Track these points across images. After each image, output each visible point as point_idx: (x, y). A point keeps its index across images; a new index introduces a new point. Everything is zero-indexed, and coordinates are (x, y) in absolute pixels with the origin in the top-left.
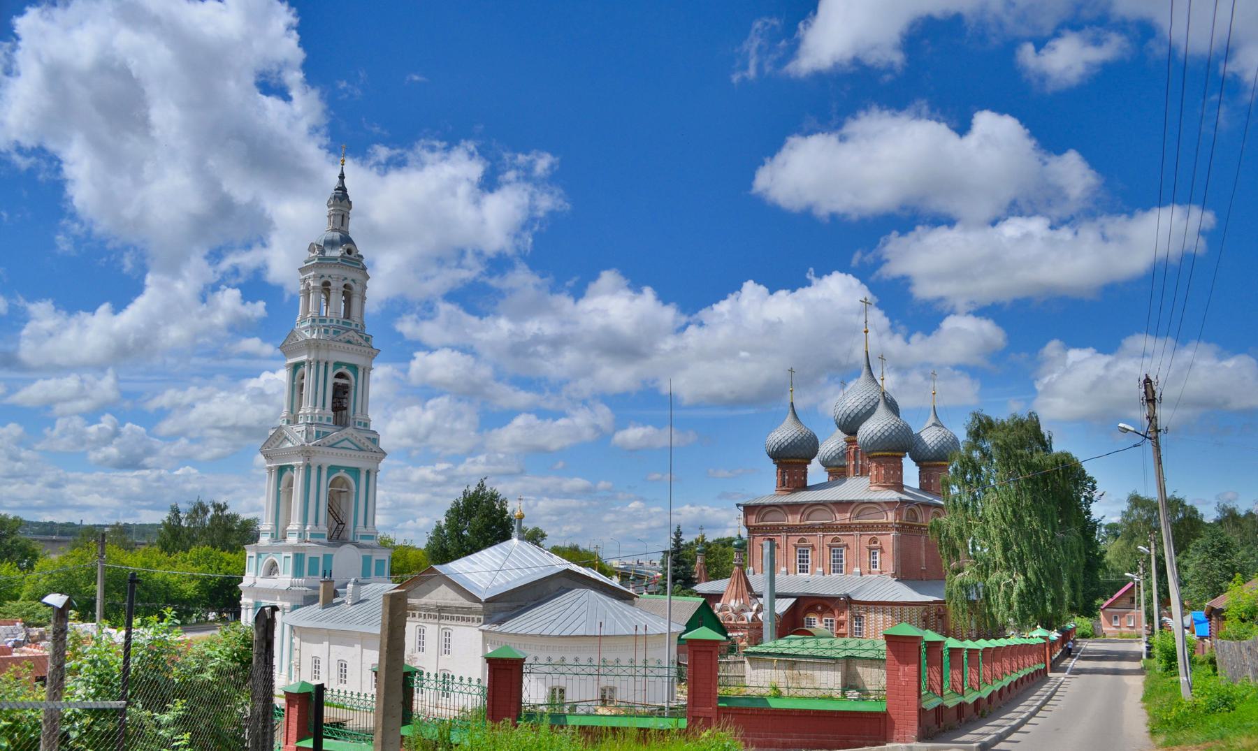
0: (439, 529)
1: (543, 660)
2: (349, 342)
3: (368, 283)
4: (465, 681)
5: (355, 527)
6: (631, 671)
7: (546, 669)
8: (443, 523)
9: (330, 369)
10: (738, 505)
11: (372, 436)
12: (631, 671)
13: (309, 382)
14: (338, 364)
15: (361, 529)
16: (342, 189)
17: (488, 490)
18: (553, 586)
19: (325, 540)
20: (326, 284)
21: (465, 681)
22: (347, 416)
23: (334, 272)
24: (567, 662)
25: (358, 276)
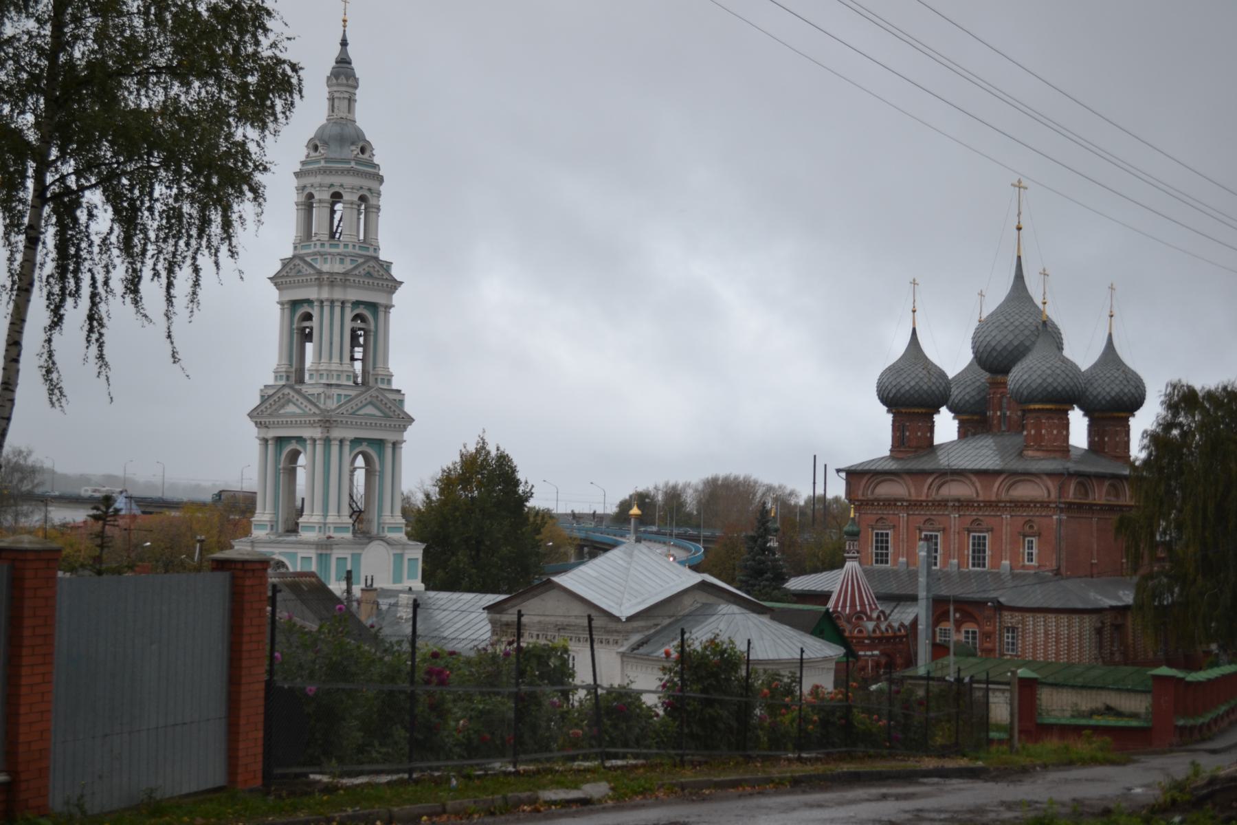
2: (369, 275)
10: (838, 471)
11: (397, 397)
14: (357, 304)
16: (343, 62)
19: (348, 535)
23: (348, 181)
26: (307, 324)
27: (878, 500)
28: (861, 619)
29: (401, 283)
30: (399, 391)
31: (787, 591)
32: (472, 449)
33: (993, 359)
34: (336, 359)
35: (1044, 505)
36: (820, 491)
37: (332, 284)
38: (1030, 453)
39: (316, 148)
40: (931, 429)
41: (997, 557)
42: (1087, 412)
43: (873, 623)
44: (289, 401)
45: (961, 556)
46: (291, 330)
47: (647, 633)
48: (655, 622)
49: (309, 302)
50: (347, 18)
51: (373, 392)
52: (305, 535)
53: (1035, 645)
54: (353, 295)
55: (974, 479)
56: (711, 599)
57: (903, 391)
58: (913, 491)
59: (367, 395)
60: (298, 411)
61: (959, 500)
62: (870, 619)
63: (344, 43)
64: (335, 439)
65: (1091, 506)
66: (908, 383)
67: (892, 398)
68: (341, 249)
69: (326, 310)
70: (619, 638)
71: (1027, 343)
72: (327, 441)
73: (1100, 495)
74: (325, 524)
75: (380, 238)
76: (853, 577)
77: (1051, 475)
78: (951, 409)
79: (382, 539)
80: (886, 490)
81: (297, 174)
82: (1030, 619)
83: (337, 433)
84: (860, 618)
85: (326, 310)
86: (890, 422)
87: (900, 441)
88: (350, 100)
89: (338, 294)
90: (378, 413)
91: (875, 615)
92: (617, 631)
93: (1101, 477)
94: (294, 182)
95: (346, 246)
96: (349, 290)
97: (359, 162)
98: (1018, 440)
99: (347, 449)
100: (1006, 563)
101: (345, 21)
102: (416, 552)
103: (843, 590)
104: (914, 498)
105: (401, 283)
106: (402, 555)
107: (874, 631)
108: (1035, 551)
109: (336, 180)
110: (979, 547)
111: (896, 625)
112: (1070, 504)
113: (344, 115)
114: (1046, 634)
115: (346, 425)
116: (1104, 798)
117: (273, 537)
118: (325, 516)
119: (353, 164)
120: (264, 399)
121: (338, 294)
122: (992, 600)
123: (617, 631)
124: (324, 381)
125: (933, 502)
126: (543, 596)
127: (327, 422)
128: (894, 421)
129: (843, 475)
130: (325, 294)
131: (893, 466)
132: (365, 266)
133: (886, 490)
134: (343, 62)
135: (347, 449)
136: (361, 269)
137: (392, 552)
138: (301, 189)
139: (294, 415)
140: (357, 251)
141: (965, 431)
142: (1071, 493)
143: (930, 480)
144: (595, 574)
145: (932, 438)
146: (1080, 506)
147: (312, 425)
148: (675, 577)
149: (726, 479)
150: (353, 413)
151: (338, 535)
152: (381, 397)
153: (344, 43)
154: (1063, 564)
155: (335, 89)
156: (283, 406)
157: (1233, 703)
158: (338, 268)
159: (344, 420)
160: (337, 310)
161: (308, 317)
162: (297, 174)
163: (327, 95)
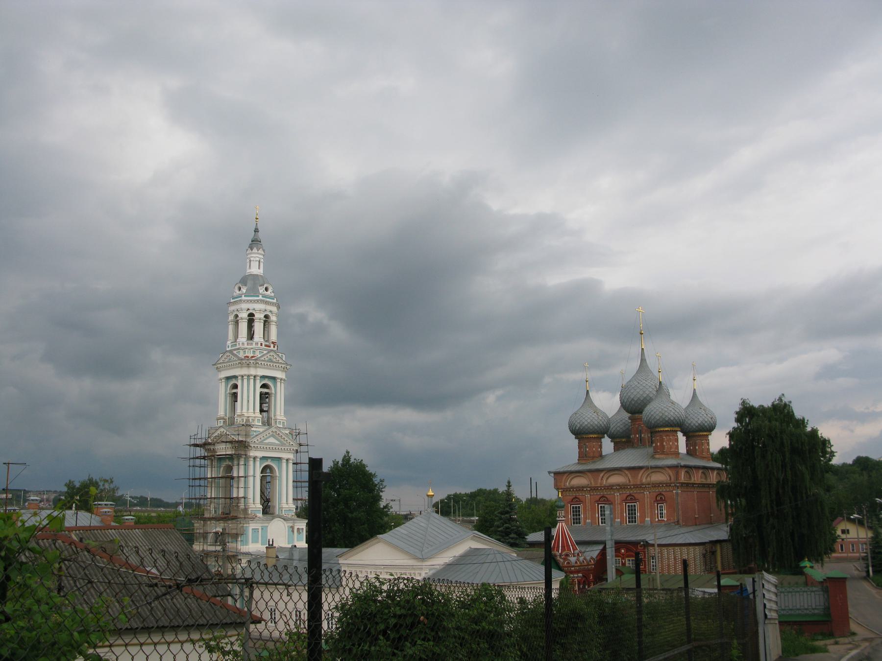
9: (258, 381)
10: (550, 472)
14: (263, 377)
26: (235, 391)
27: (572, 488)
33: (633, 408)
34: (251, 410)
35: (668, 485)
36: (534, 495)
38: (657, 456)
40: (601, 447)
41: (643, 517)
42: (685, 434)
43: (575, 558)
45: (622, 517)
49: (235, 377)
51: (273, 429)
53: (669, 565)
54: (261, 372)
55: (627, 472)
59: (270, 431)
61: (619, 485)
65: (693, 484)
67: (579, 433)
68: (254, 346)
69: (245, 381)
71: (651, 395)
73: (697, 478)
77: (670, 467)
78: (609, 437)
82: (665, 550)
85: (245, 381)
87: (583, 456)
89: (252, 371)
90: (277, 442)
93: (697, 468)
95: (257, 344)
96: (258, 369)
98: (651, 450)
99: (258, 463)
100: (648, 519)
102: (302, 524)
104: (593, 485)
106: (292, 527)
108: (665, 512)
110: (632, 511)
111: (588, 558)
112: (682, 484)
114: (675, 558)
116: (274, 507)
122: (643, 541)
125: (605, 486)
135: (258, 463)
137: (286, 525)
141: (617, 448)
142: (683, 478)
143: (602, 475)
144: (405, 532)
145: (601, 451)
146: (687, 484)
154: (681, 518)
160: (252, 381)
161: (235, 386)
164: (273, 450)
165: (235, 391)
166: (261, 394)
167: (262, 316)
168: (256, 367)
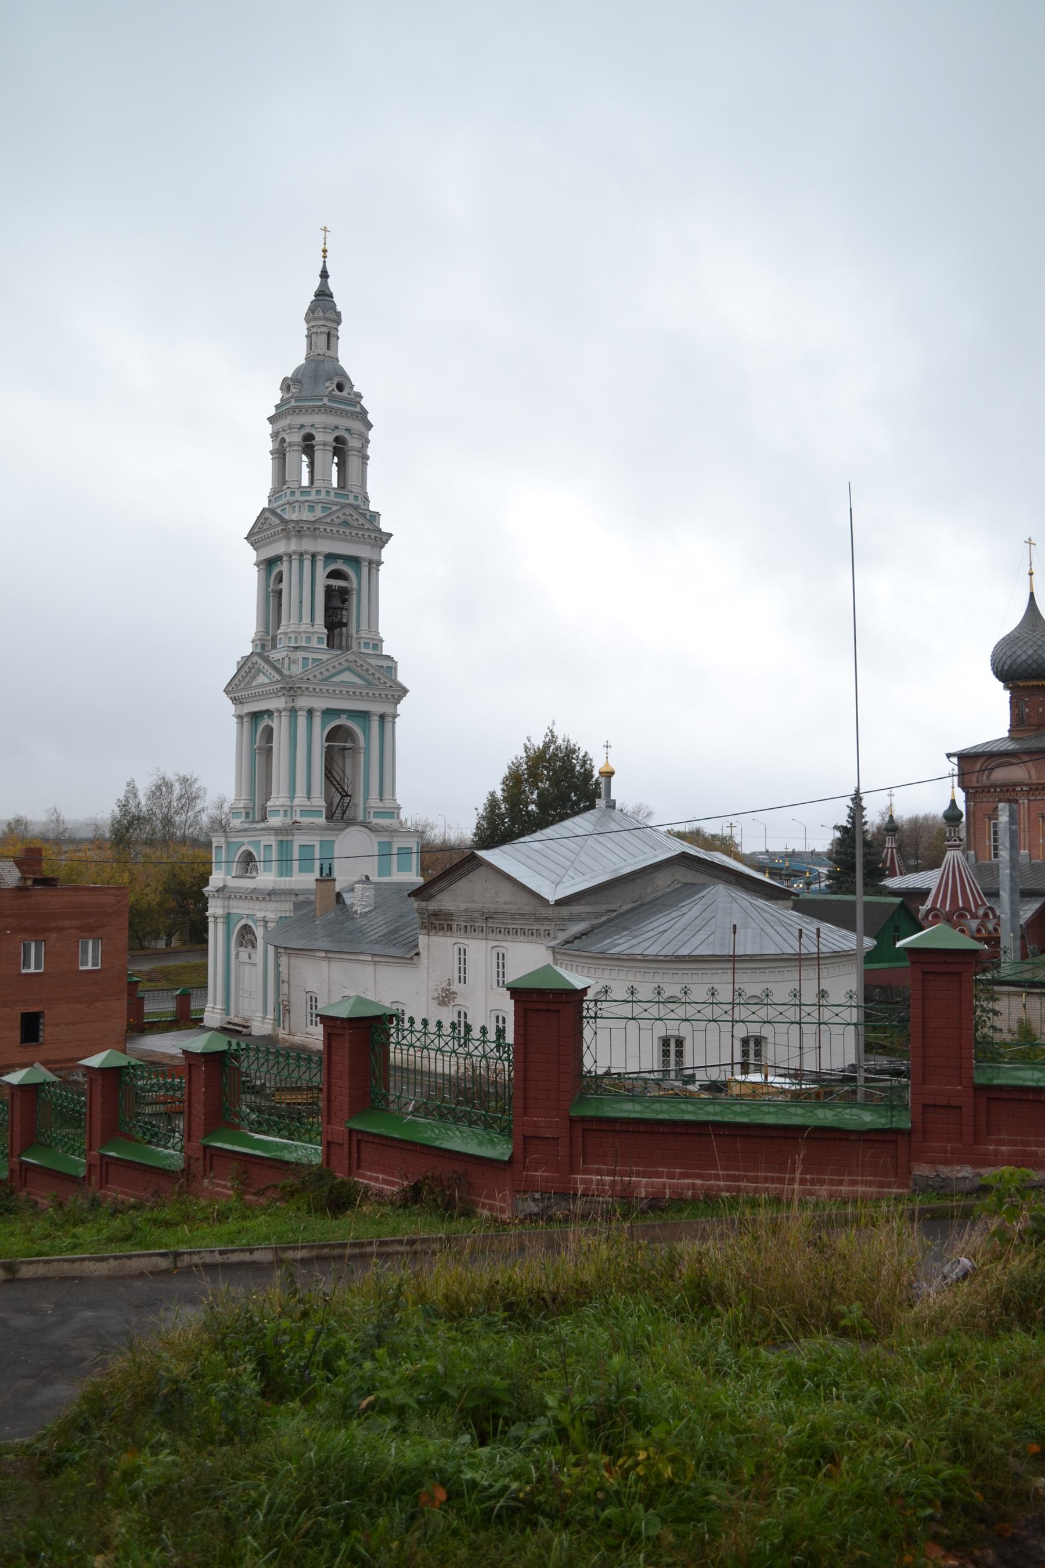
0: (493, 804)
1: (619, 992)
2: (345, 524)
3: (372, 435)
4: (432, 1028)
5: (366, 800)
6: (791, 1014)
7: (626, 1010)
8: (499, 794)
9: (320, 564)
10: (949, 756)
11: (385, 663)
12: (791, 1014)
13: (290, 588)
14: (330, 557)
15: (374, 802)
16: (324, 295)
17: (560, 742)
18: (663, 881)
19: (322, 820)
20: (309, 437)
21: (432, 1028)
22: (348, 635)
23: (320, 419)
24: (693, 997)
25: (356, 425)
27: (994, 786)
28: (964, 916)
29: (391, 535)
30: (389, 658)
31: (885, 887)
32: (539, 742)
34: (306, 619)
37: (299, 534)
39: (289, 387)
44: (259, 671)
46: (267, 594)
47: (595, 922)
48: (611, 907)
50: (327, 248)
52: (274, 821)
54: (326, 546)
56: (700, 878)
57: (1019, 661)
58: (1033, 773)
60: (267, 681)
62: (974, 916)
63: (324, 275)
64: (301, 709)
66: (1024, 654)
70: (551, 927)
72: (293, 712)
74: (292, 807)
75: (371, 489)
76: (956, 869)
79: (366, 825)
80: (1002, 775)
81: (271, 420)
83: (303, 702)
84: (962, 916)
85: (295, 564)
86: (1008, 700)
88: (329, 334)
89: (308, 545)
90: (359, 681)
91: (981, 912)
92: (547, 919)
94: (269, 428)
97: (332, 398)
101: (325, 251)
103: (943, 884)
104: (1035, 781)
105: (391, 535)
107: (979, 931)
109: (306, 419)
113: (321, 352)
115: (314, 693)
117: (246, 826)
118: (292, 798)
119: (326, 401)
120: (812, 852)
121: (308, 545)
123: (547, 919)
124: (292, 644)
126: (470, 876)
127: (291, 690)
128: (1011, 698)
129: (955, 760)
130: (293, 546)
131: (1011, 746)
132: (340, 514)
133: (1002, 775)
134: (324, 295)
135: (317, 721)
136: (334, 517)
138: (275, 435)
139: (264, 685)
140: (332, 497)
147: (276, 694)
148: (647, 849)
149: (926, 818)
150: (326, 679)
151: (306, 820)
152: (360, 662)
153: (324, 275)
155: (312, 324)
156: (254, 678)
157: (3, 1442)
158: (306, 515)
159: (304, 686)
160: (307, 564)
162: (271, 420)
163: (306, 332)
164: (348, 696)
165: (542, 932)
166: (329, 591)
167: (330, 439)
168: (315, 537)
